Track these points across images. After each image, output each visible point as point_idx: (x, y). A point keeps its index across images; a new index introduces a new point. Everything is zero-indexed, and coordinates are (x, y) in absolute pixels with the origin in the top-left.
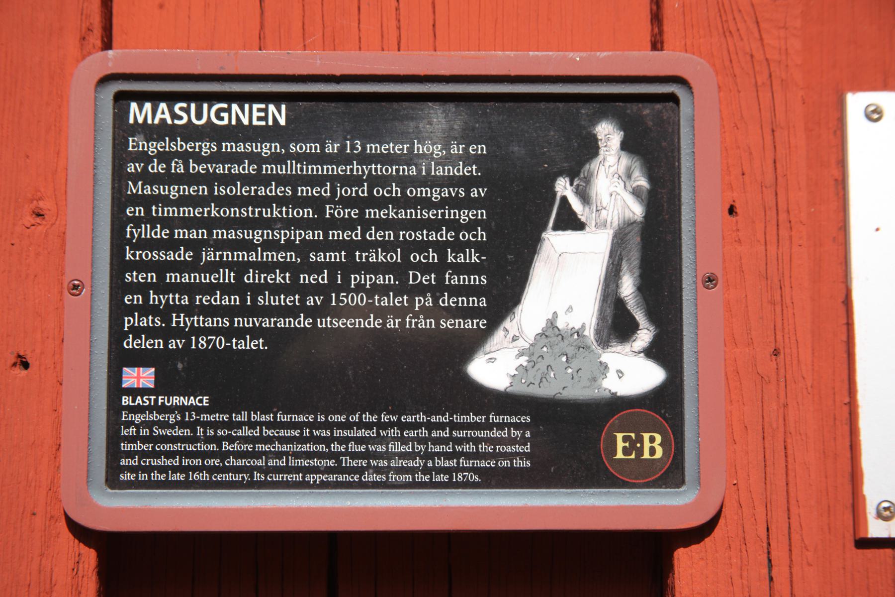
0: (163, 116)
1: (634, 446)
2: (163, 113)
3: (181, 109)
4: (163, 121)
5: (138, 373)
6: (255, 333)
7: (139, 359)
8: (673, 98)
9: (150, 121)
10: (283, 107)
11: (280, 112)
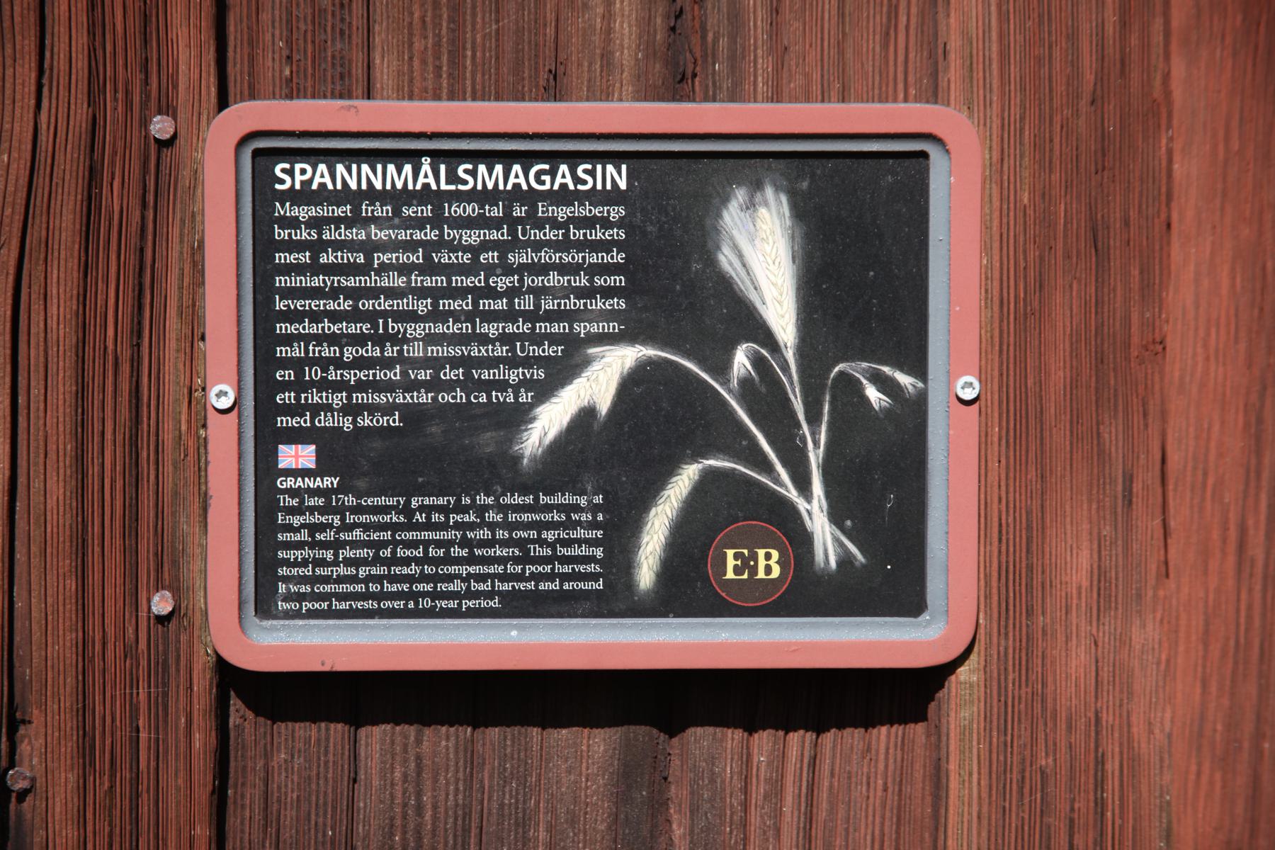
0: (322, 180)
1: (747, 564)
2: (564, 176)
3: (585, 171)
4: (564, 186)
5: (296, 452)
6: (388, 410)
7: (296, 436)
8: (924, 155)
9: (410, 187)
10: (624, 167)
11: (620, 173)
